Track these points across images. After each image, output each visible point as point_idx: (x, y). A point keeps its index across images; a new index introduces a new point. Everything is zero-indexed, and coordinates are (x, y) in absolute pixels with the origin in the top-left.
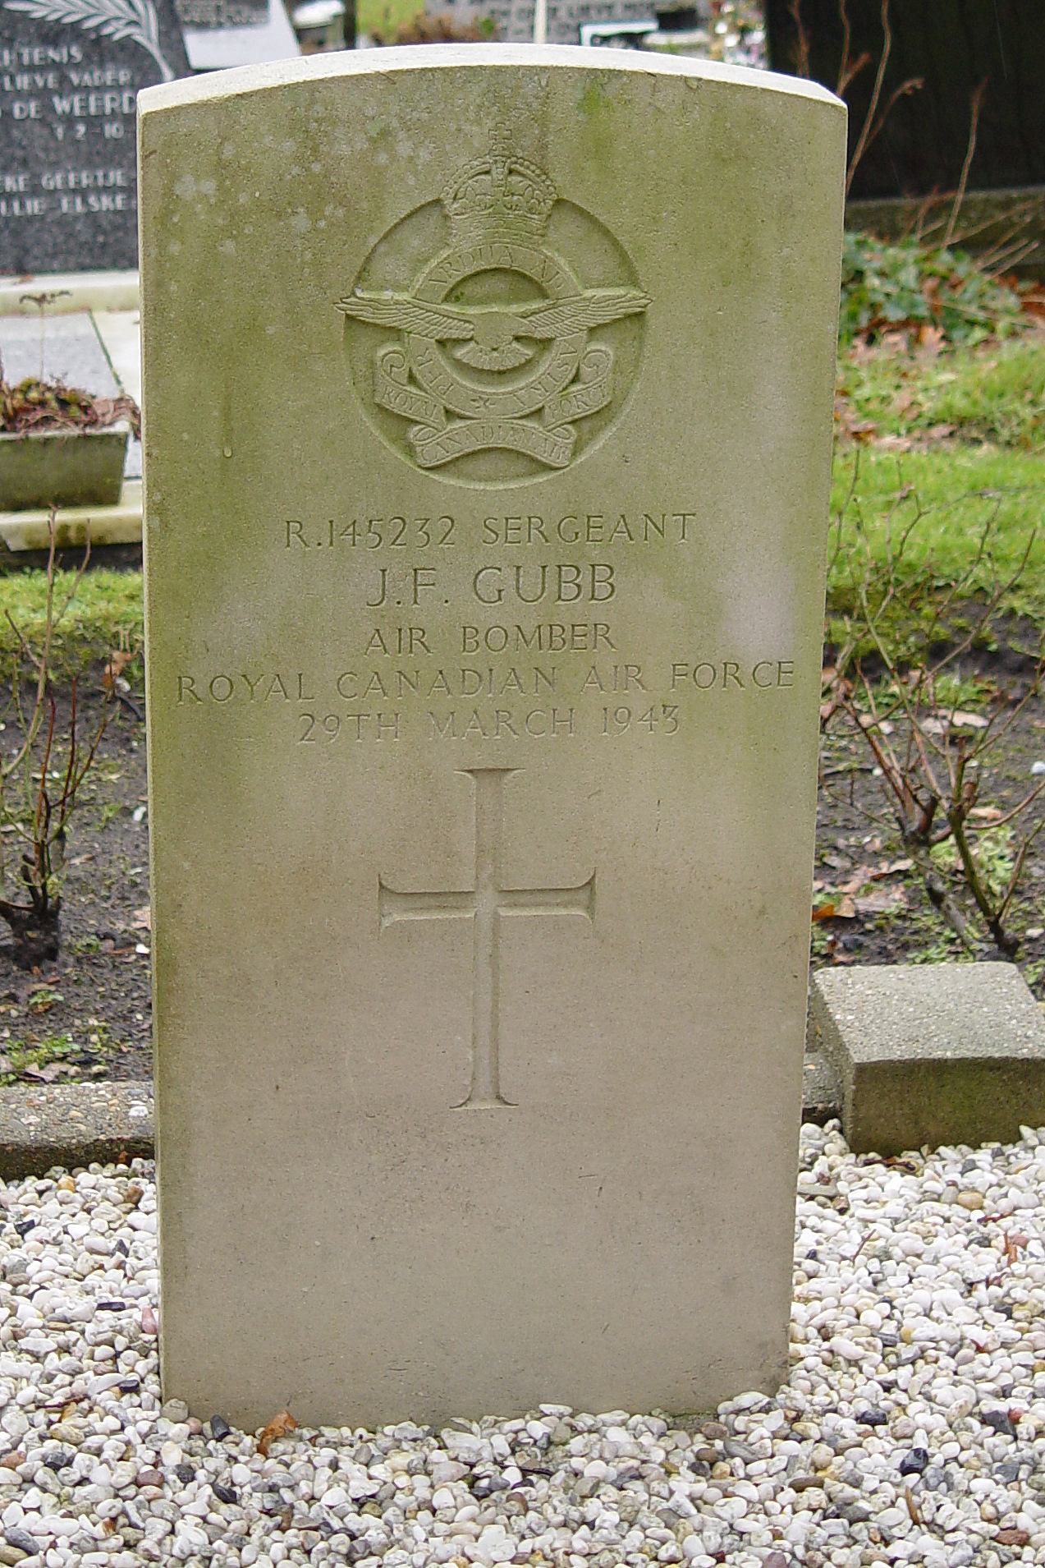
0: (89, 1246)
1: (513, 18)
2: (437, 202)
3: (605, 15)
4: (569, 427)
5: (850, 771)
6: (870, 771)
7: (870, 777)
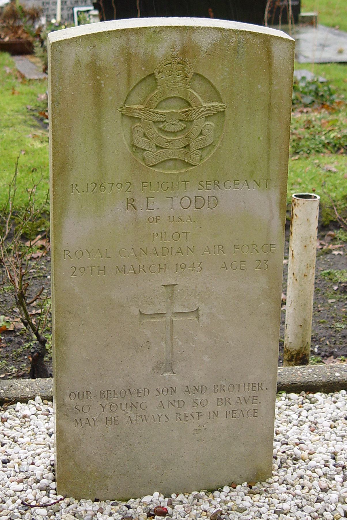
0: (33, 432)
1: (51, 5)
2: (153, 74)
3: (84, 4)
4: (198, 151)
5: (39, 277)
6: (46, 276)
7: (46, 279)
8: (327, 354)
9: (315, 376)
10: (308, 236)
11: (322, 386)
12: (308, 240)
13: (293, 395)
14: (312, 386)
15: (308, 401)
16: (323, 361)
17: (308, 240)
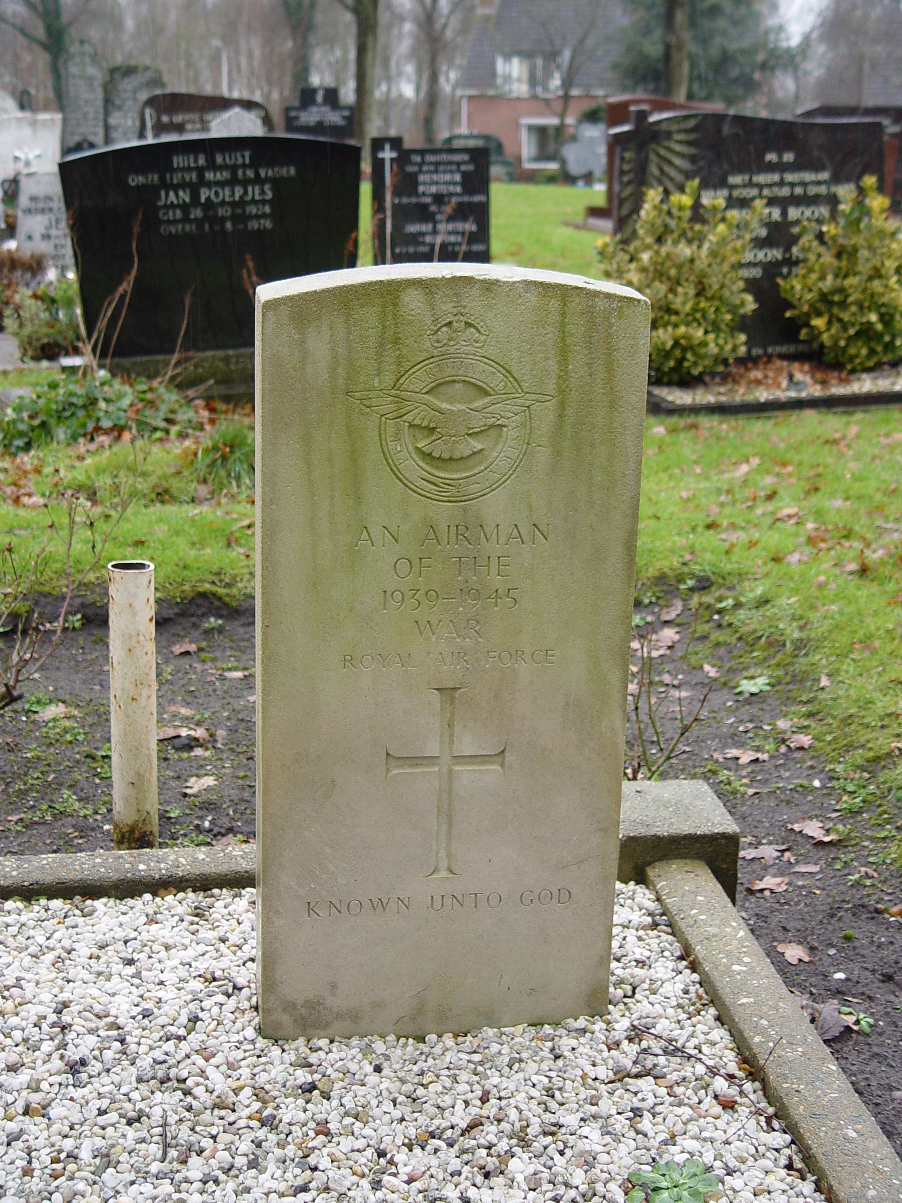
8: (223, 831)
9: (103, 870)
10: (134, 633)
11: (111, 887)
12: (134, 639)
13: (57, 904)
14: (95, 887)
15: (77, 912)
16: (214, 843)
17: (134, 639)
